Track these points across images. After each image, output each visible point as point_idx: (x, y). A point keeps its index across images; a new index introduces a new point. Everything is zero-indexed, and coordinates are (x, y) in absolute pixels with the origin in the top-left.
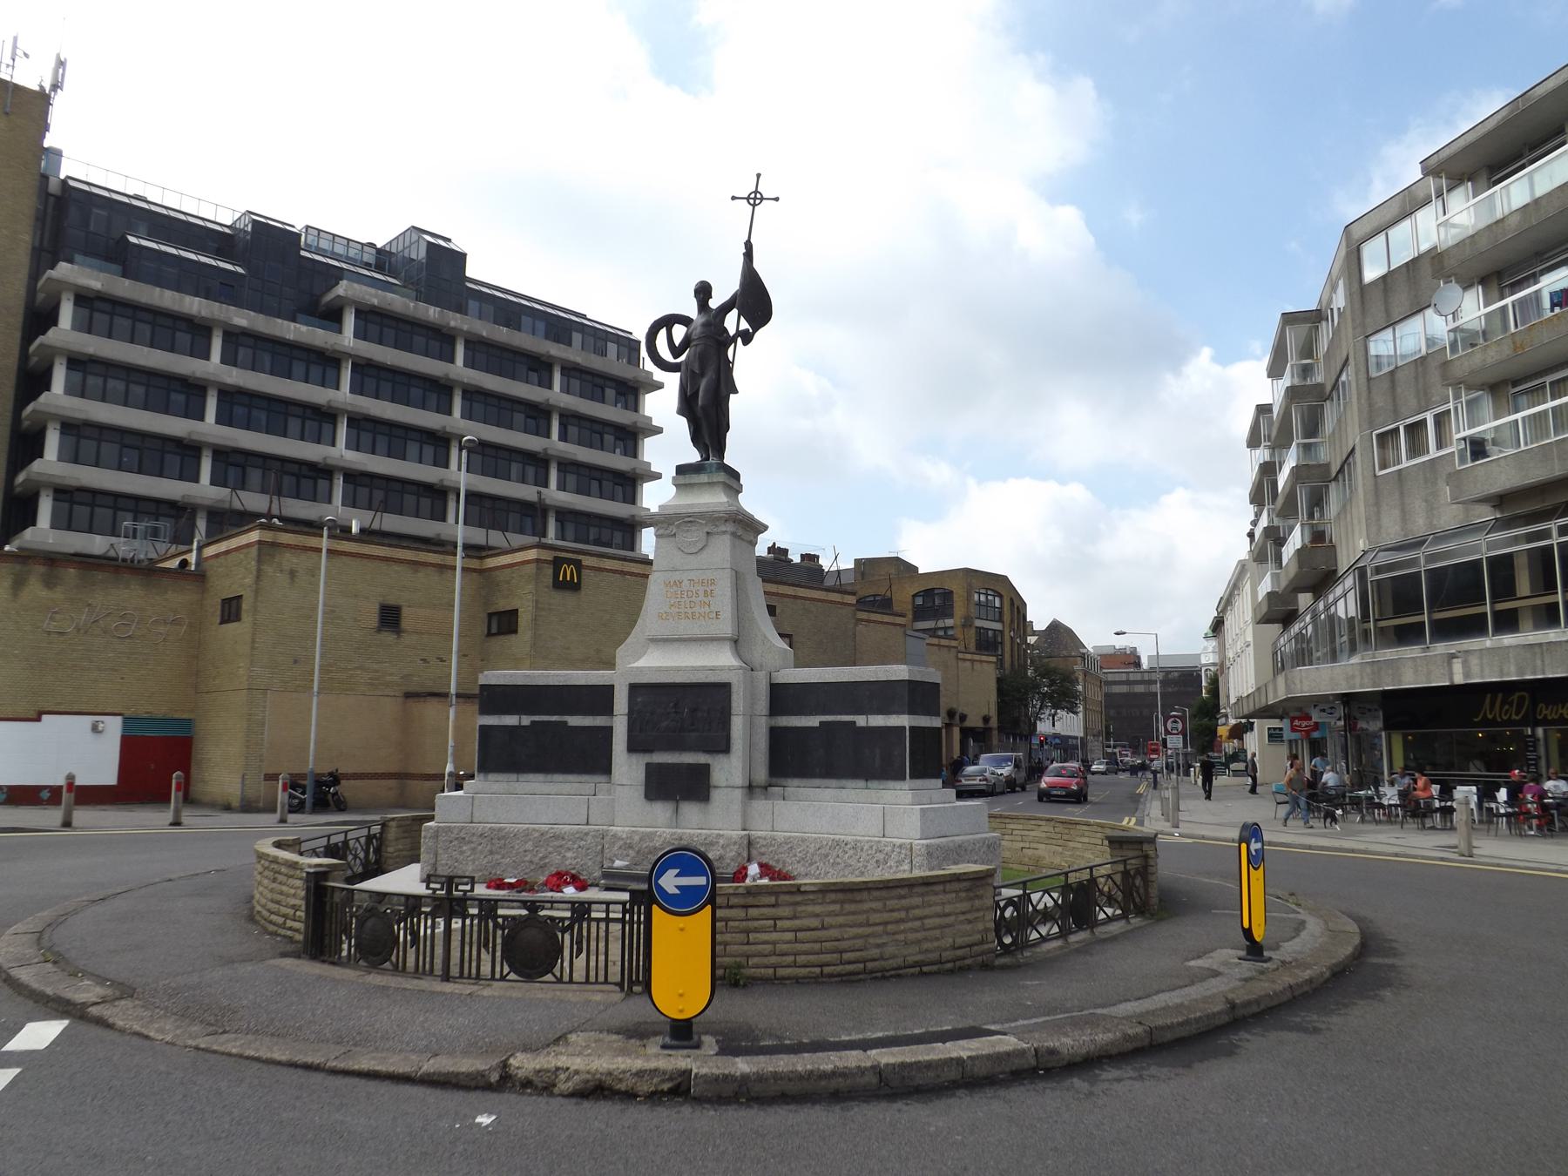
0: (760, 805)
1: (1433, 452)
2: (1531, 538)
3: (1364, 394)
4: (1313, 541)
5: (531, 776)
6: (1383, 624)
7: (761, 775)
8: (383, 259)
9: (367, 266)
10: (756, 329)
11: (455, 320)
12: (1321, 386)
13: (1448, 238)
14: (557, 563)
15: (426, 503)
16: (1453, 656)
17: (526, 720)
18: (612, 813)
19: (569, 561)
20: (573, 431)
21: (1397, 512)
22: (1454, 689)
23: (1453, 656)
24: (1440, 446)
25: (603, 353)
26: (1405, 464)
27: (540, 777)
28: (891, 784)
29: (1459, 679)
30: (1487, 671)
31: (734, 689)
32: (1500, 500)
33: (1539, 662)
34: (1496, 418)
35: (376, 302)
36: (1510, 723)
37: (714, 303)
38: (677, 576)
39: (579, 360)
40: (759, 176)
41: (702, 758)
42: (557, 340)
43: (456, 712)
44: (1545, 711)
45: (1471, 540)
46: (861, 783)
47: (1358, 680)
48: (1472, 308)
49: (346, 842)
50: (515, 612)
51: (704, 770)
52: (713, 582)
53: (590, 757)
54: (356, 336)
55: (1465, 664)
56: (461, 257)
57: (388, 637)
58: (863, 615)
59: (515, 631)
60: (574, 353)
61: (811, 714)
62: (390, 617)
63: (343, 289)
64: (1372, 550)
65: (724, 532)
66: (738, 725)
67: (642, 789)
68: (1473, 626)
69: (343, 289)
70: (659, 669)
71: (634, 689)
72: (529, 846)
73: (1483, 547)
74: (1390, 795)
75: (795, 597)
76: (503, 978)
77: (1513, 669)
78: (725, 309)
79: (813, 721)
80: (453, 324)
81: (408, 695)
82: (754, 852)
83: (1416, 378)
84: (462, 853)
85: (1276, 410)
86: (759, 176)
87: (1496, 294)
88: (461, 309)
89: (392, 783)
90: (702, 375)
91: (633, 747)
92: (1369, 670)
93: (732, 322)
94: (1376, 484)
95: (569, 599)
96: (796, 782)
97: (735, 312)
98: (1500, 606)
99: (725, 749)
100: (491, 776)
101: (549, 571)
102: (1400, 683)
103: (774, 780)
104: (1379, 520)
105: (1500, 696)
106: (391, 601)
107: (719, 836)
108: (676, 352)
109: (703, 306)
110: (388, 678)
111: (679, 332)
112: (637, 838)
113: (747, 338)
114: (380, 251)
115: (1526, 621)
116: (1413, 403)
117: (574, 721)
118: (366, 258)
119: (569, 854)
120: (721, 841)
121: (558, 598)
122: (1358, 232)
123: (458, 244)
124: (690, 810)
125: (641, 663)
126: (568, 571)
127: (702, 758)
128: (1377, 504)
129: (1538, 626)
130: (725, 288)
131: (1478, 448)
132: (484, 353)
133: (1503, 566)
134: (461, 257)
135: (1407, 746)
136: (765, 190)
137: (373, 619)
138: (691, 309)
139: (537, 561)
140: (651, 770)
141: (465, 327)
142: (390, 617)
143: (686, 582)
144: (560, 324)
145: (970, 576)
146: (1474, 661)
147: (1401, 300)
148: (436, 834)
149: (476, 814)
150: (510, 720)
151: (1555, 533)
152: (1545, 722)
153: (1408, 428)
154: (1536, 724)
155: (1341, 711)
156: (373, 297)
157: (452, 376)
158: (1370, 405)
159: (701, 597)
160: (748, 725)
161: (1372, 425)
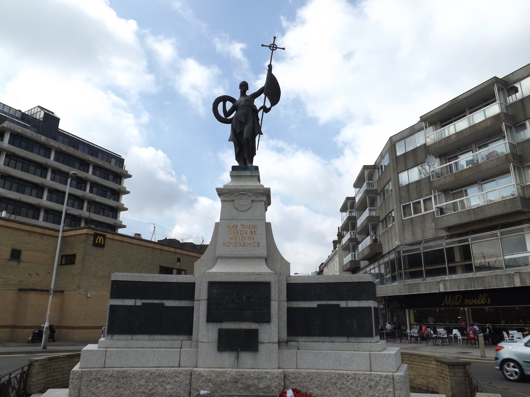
0: (288, 353)
1: (423, 212)
2: (460, 242)
3: (398, 192)
4: (374, 242)
5: (140, 337)
6: (406, 271)
7: (284, 335)
8: (24, 117)
9: (17, 118)
11: (52, 143)
12: (376, 190)
13: (429, 141)
14: (95, 236)
15: (31, 212)
16: (439, 282)
17: (139, 303)
19: (101, 235)
20: (95, 189)
21: (411, 232)
22: (440, 294)
23: (439, 282)
24: (425, 210)
25: (110, 162)
26: (413, 216)
27: (147, 337)
28: (364, 339)
29: (442, 290)
30: (453, 287)
31: (272, 286)
32: (449, 229)
33: (473, 284)
34: (446, 202)
35: (20, 131)
36: (455, 306)
37: (249, 93)
38: (234, 223)
39: (100, 163)
41: (253, 326)
42: (92, 155)
43: (53, 297)
44: (467, 301)
45: (439, 242)
46: (345, 339)
47: (403, 291)
48: (435, 165)
49: (9, 381)
50: (74, 256)
51: (254, 333)
52: (255, 227)
53: (179, 324)
54: (9, 143)
55: (445, 285)
56: (58, 120)
57: (14, 263)
59: (74, 264)
60: (98, 161)
61: (312, 300)
62: (16, 255)
63: (6, 124)
64: (402, 245)
65: (262, 201)
66: (274, 305)
67: (215, 345)
68: (442, 272)
69: (6, 124)
70: (227, 274)
71: (212, 285)
72: (143, 382)
73: (444, 244)
74: (415, 331)
75: (188, 255)
77: (463, 286)
78: (257, 95)
79: (313, 304)
80: (51, 144)
81: (20, 290)
82: (287, 382)
83: (417, 187)
84: (97, 388)
85: (357, 200)
87: (444, 161)
88: (55, 139)
89: (7, 330)
90: (246, 123)
91: (211, 319)
92: (407, 287)
93: (258, 103)
94: (403, 223)
95: (99, 251)
96: (304, 339)
97: (263, 95)
98: (451, 265)
99: (267, 320)
100: (116, 337)
101: (92, 239)
102: (419, 291)
103: (290, 338)
104: (404, 235)
105: (451, 296)
106: (17, 247)
107: (267, 372)
108: (227, 114)
109: (243, 93)
110: (12, 282)
111: (229, 105)
113: (266, 110)
114: (23, 114)
115: (459, 270)
116: (416, 195)
117: (169, 303)
118: (17, 115)
119: (168, 387)
121: (95, 250)
122: (394, 140)
123: (57, 114)
124: (246, 357)
125: (214, 270)
126: (100, 239)
127: (253, 326)
128: (403, 229)
129: (463, 272)
130: (259, 82)
131: (441, 211)
132: (62, 156)
133: (450, 251)
134: (58, 120)
135: (415, 314)
137: (8, 255)
138: (237, 96)
139: (87, 234)
140: (220, 331)
141: (56, 146)
142: (16, 255)
143: (239, 226)
144: (94, 150)
146: (448, 284)
147: (410, 161)
148: (80, 375)
149: (108, 362)
150: (129, 302)
152: (468, 306)
153: (424, 201)
154: (464, 306)
156: (19, 129)
157: (48, 163)
158: (400, 196)
159: (249, 235)
160: (278, 306)
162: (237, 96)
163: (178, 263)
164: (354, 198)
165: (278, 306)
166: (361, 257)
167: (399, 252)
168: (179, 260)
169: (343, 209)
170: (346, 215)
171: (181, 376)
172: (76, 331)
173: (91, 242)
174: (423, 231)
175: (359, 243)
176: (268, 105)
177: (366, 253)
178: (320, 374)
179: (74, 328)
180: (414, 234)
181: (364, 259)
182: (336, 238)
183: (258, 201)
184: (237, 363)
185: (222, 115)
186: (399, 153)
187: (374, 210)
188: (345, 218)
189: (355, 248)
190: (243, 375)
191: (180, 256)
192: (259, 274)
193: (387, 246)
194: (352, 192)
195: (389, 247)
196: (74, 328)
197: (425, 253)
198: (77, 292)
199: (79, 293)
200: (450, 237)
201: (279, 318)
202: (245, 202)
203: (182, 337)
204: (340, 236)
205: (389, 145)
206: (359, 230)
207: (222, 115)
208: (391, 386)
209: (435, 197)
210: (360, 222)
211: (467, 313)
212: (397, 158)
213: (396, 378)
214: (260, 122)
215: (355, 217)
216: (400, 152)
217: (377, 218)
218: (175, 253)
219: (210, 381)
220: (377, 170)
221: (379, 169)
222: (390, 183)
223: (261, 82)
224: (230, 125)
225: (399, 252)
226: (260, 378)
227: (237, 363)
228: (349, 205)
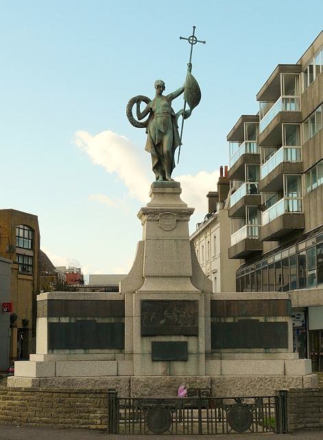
0: (215, 364)
10: (192, 109)
53: (111, 338)
76: (228, 433)
91: (144, 334)
93: (178, 105)
99: (195, 334)
108: (141, 116)
109: (160, 94)
111: (143, 106)
112: (151, 381)
113: (186, 115)
127: (183, 339)
130: (174, 83)
136: (189, 34)
138: (152, 94)
140: (154, 344)
149: (57, 372)
160: (204, 324)
162: (152, 94)
164: (256, 119)
166: (265, 235)
170: (239, 150)
171: (121, 383)
176: (188, 108)
177: (276, 228)
181: (271, 238)
182: (215, 189)
183: (182, 221)
185: (136, 119)
187: (293, 100)
188: (238, 157)
190: (176, 381)
193: (313, 219)
194: (254, 108)
203: (117, 351)
204: (225, 185)
206: (262, 138)
207: (136, 119)
210: (267, 169)
214: (179, 130)
215: (257, 156)
217: (299, 166)
220: (302, 73)
221: (306, 72)
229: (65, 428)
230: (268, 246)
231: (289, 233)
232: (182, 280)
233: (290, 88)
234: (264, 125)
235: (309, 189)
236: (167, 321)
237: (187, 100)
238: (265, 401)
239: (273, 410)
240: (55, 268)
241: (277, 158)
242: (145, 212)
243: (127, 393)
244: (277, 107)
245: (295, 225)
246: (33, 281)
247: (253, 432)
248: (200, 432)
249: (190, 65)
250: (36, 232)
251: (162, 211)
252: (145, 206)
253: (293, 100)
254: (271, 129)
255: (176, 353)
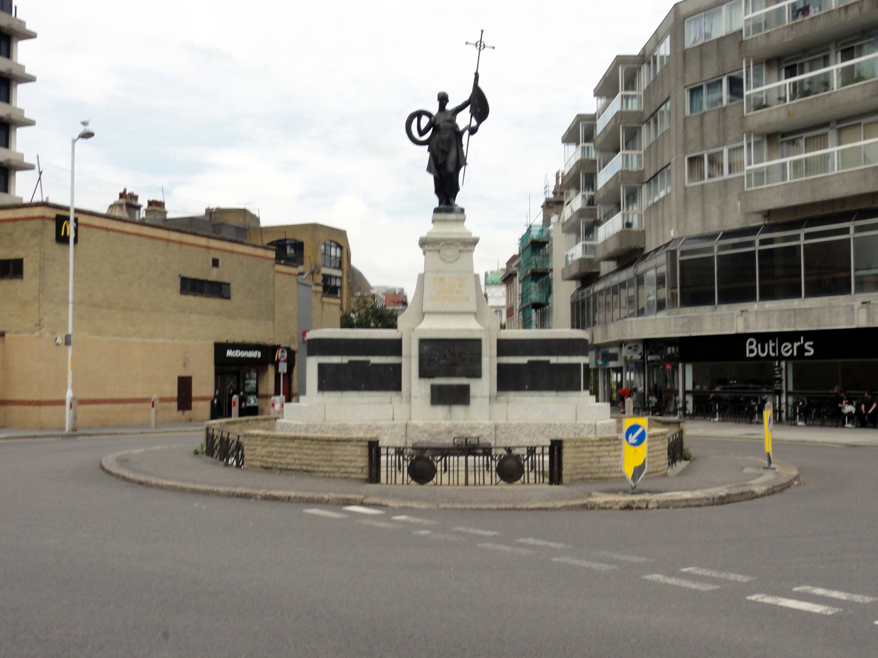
3: (681, 128)
18: (405, 414)
21: (699, 214)
24: (730, 172)
26: (707, 180)
40: (482, 31)
41: (464, 381)
53: (389, 380)
58: (279, 268)
67: (428, 399)
71: (423, 342)
75: (232, 252)
76: (497, 484)
85: (601, 125)
86: (482, 31)
93: (464, 119)
101: (52, 226)
108: (422, 133)
111: (425, 121)
113: (473, 131)
120: (481, 427)
127: (464, 381)
130: (459, 95)
138: (434, 109)
139: (43, 218)
145: (315, 228)
146: (752, 318)
151: (802, 237)
155: (640, 349)
160: (489, 361)
161: (685, 151)
163: (215, 270)
164: (593, 118)
165: (489, 361)
166: (600, 254)
167: (673, 253)
168: (215, 263)
169: (571, 137)
170: (571, 155)
172: (44, 409)
173: (53, 235)
174: (722, 213)
175: (598, 223)
176: (474, 123)
177: (612, 248)
178: (528, 424)
179: (39, 403)
180: (704, 218)
181: (609, 258)
184: (450, 416)
186: (689, 43)
188: (573, 162)
189: (590, 230)
191: (217, 255)
192: (470, 330)
193: (653, 235)
194: (591, 105)
195: (657, 239)
196: (39, 403)
197: (719, 257)
198: (37, 334)
199: (41, 336)
200: (768, 228)
201: (490, 373)
202: (451, 252)
205: (671, 21)
206: (598, 141)
208: (593, 432)
209: (749, 145)
210: (603, 178)
211: (784, 371)
212: (685, 52)
213: (598, 426)
216: (692, 37)
218: (208, 248)
219: (425, 431)
221: (649, 63)
222: (669, 104)
223: (466, 94)
224: (426, 147)
225: (673, 253)
226: (473, 428)
227: (450, 416)
228: (581, 131)
229: (324, 477)
230: (606, 267)
231: (629, 255)
232: (464, 318)
233: (630, 83)
234: (601, 125)
235: (650, 202)
236: (448, 362)
237: (473, 113)
238: (539, 450)
239: (547, 458)
240: (372, 288)
241: (616, 164)
242: (423, 243)
243: (404, 439)
244: (616, 105)
245: (634, 243)
246: (341, 305)
247: (436, 484)
248: (467, 483)
249: (477, 76)
250: (345, 250)
251: (443, 240)
252: (424, 234)
253: (634, 96)
254: (608, 130)
255: (460, 396)
